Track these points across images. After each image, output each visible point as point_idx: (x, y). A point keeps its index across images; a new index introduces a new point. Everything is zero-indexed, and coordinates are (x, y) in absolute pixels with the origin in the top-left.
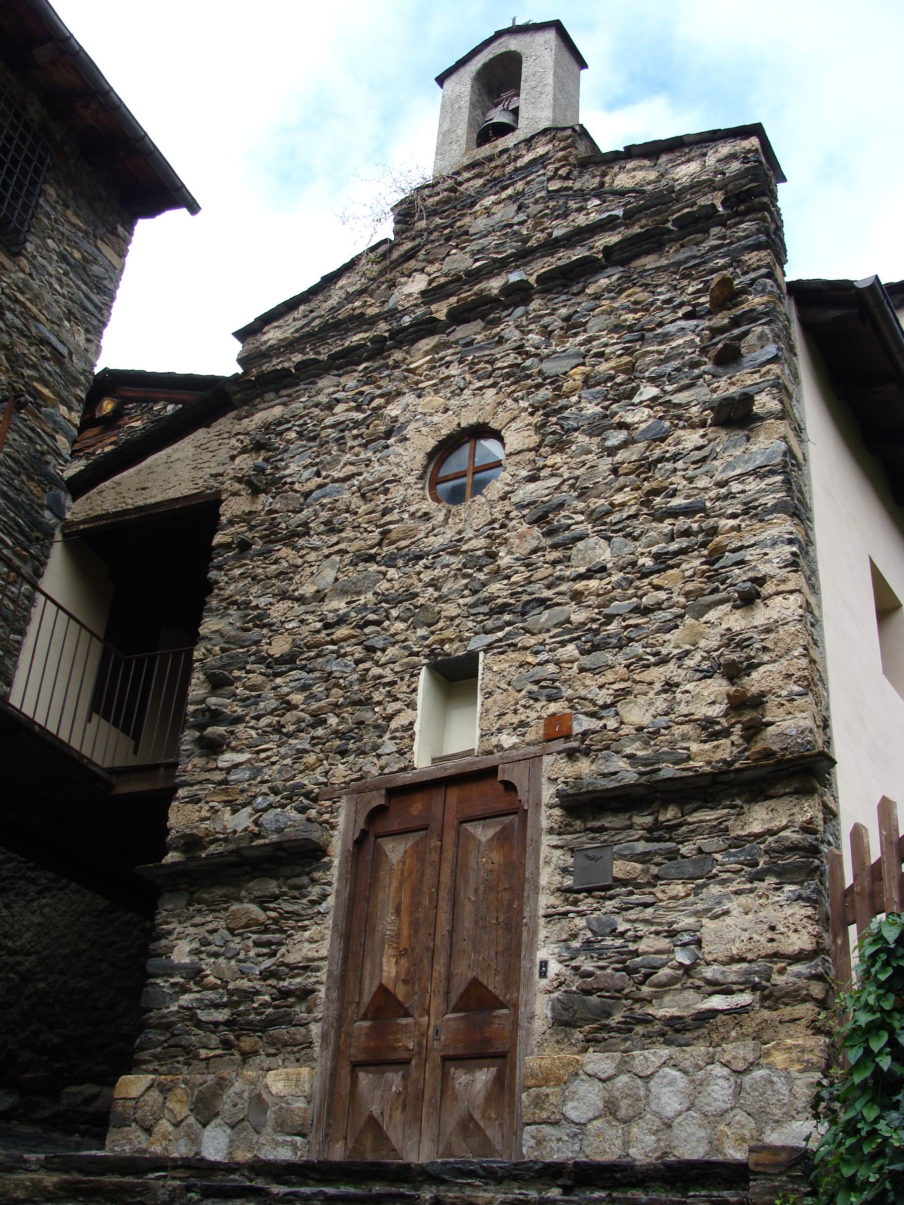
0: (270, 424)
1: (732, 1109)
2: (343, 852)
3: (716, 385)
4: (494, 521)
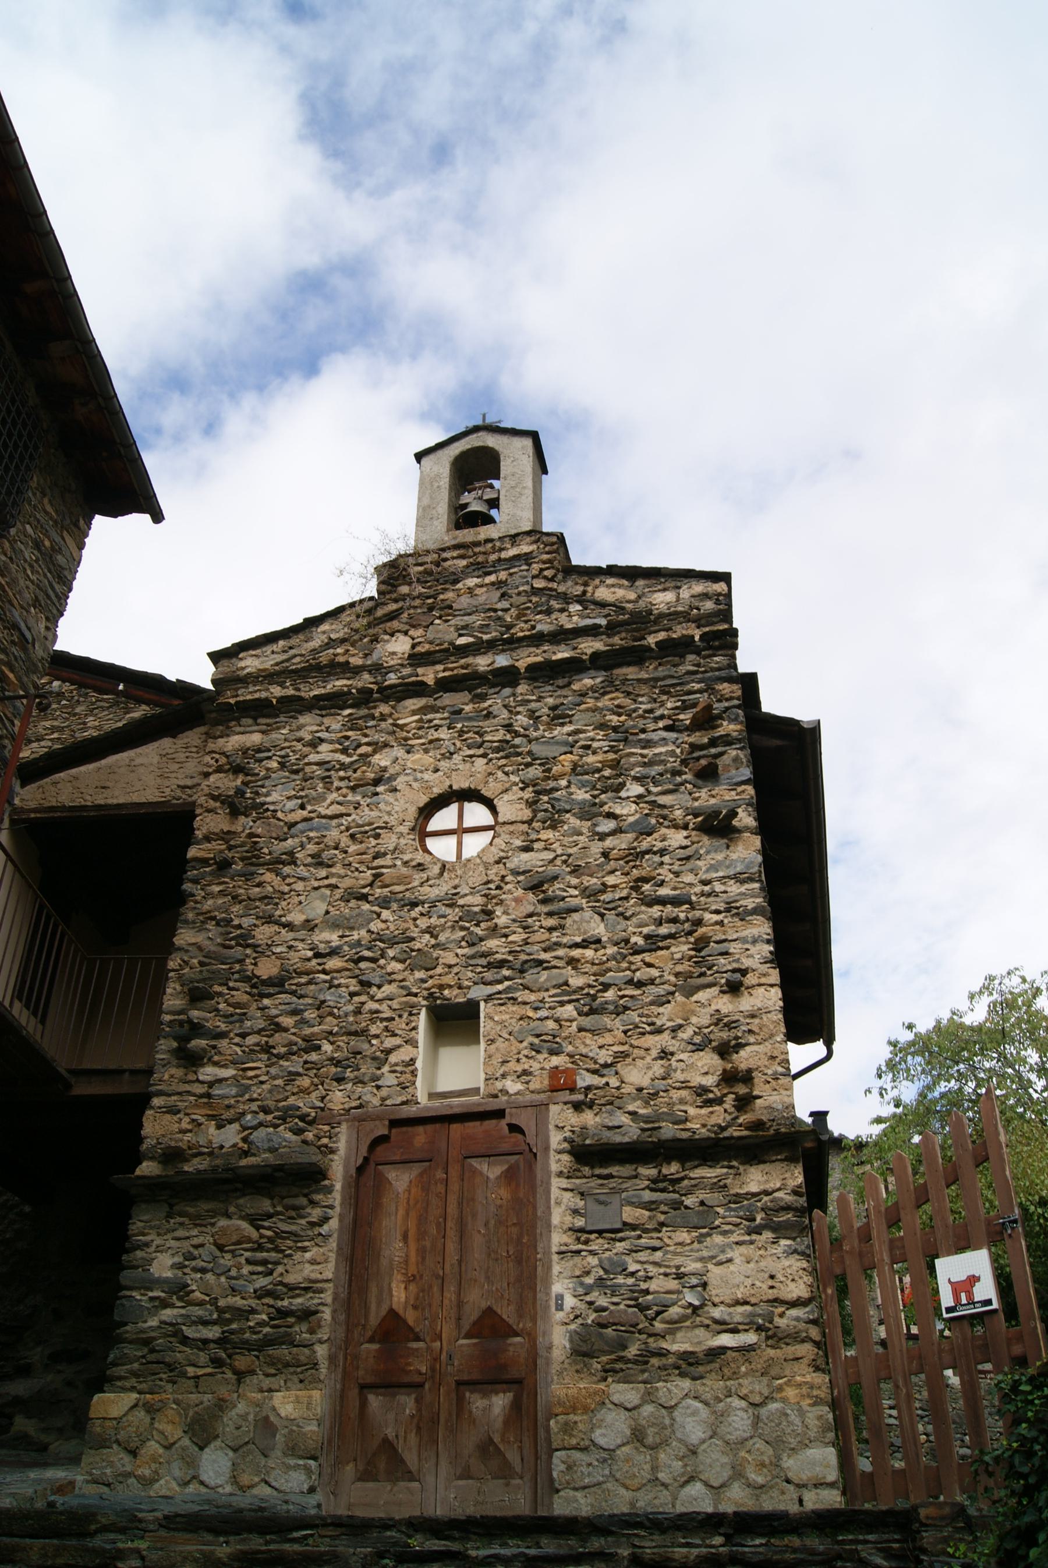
0: (248, 749)
1: (751, 1437)
2: (345, 1178)
3: (697, 795)
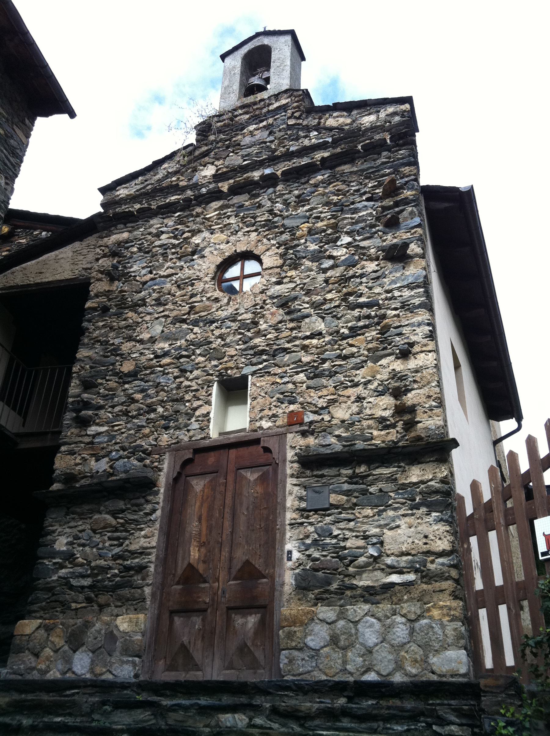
0: (121, 242)
1: (409, 642)
2: (166, 485)
3: (385, 238)
4: (256, 305)
